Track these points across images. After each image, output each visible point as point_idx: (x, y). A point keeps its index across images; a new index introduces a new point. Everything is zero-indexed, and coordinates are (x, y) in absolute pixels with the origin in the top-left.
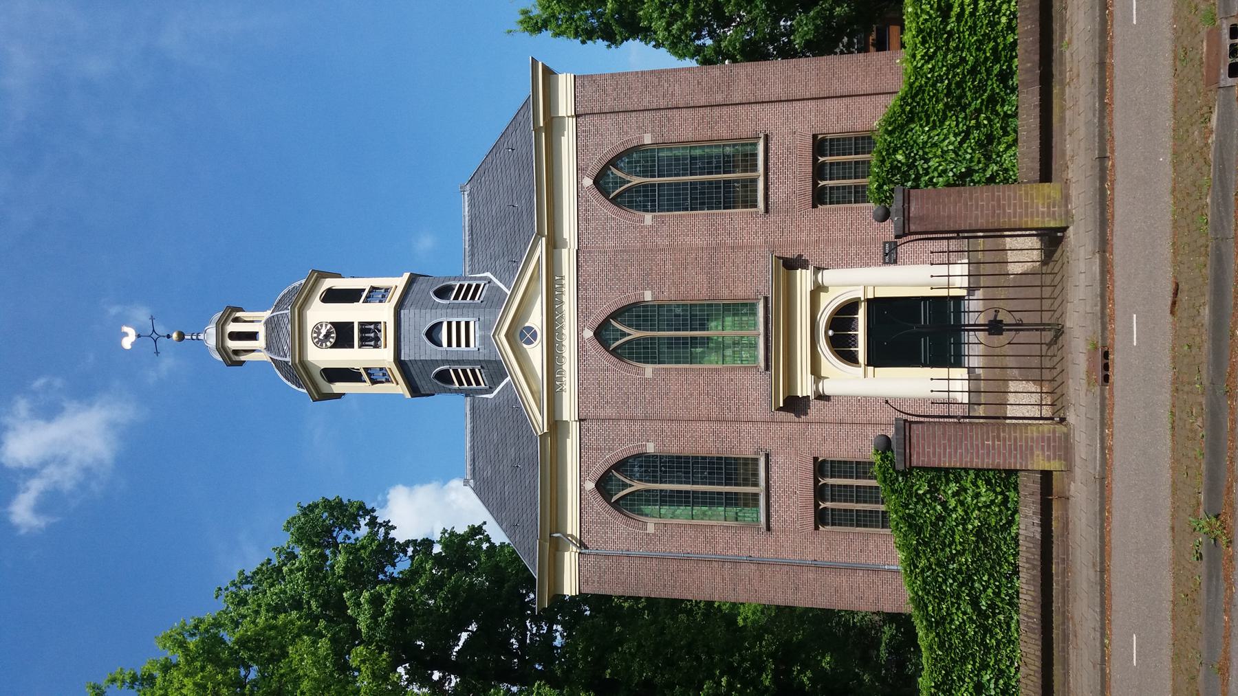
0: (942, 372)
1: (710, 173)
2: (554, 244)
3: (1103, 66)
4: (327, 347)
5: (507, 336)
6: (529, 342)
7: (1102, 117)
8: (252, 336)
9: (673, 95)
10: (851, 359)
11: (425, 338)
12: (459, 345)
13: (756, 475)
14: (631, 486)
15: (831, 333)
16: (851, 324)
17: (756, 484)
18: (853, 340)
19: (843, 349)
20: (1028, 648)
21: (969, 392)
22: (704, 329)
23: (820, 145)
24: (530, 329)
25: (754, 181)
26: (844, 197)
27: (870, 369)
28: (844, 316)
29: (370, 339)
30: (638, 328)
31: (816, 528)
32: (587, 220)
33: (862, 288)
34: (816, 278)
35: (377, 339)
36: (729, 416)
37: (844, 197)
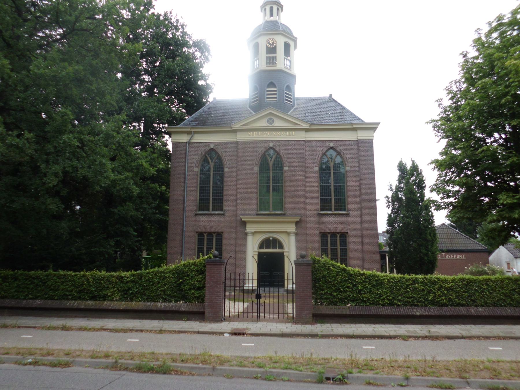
0: (256, 277)
1: (334, 192)
2: (307, 130)
3: (470, 338)
4: (266, 44)
5: (270, 113)
6: (268, 121)
7: (495, 337)
8: (272, 15)
9: (365, 178)
10: (261, 246)
11: (270, 81)
12: (268, 94)
13: (216, 210)
14: (212, 162)
15: (271, 239)
16: (274, 247)
17: (213, 210)
18: (268, 247)
19: (266, 243)
20: (123, 305)
21: (248, 289)
22: (273, 190)
23: (344, 235)
24: (273, 121)
25: (331, 210)
26: (323, 244)
27: (257, 253)
28: (276, 243)
29: (270, 60)
30: (274, 164)
31: (197, 232)
32: (316, 144)
33: (288, 251)
34: (292, 233)
35: (270, 63)
36: (239, 200)
37: (323, 244)
